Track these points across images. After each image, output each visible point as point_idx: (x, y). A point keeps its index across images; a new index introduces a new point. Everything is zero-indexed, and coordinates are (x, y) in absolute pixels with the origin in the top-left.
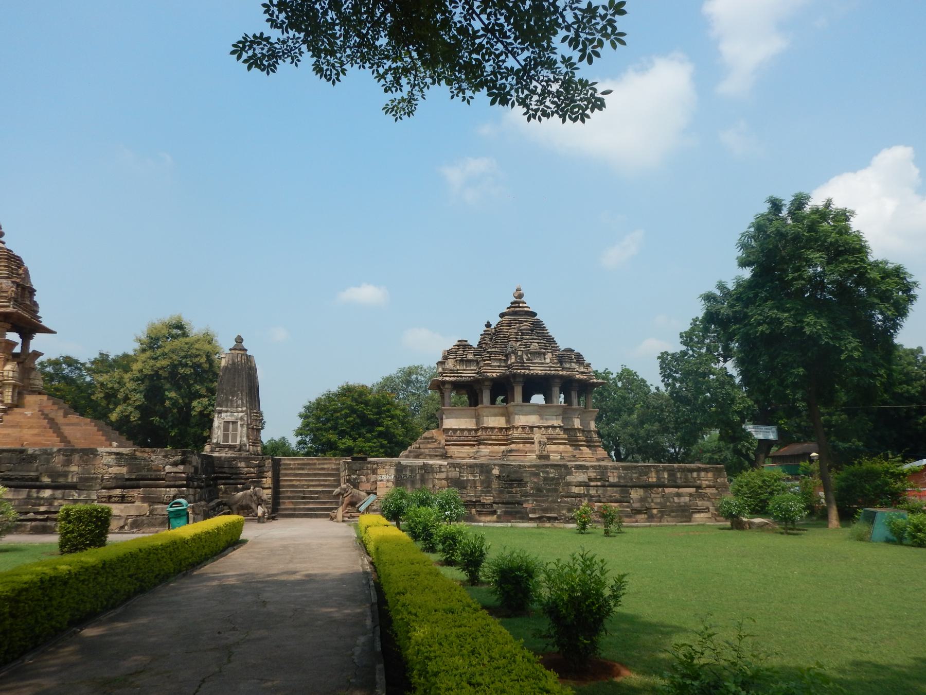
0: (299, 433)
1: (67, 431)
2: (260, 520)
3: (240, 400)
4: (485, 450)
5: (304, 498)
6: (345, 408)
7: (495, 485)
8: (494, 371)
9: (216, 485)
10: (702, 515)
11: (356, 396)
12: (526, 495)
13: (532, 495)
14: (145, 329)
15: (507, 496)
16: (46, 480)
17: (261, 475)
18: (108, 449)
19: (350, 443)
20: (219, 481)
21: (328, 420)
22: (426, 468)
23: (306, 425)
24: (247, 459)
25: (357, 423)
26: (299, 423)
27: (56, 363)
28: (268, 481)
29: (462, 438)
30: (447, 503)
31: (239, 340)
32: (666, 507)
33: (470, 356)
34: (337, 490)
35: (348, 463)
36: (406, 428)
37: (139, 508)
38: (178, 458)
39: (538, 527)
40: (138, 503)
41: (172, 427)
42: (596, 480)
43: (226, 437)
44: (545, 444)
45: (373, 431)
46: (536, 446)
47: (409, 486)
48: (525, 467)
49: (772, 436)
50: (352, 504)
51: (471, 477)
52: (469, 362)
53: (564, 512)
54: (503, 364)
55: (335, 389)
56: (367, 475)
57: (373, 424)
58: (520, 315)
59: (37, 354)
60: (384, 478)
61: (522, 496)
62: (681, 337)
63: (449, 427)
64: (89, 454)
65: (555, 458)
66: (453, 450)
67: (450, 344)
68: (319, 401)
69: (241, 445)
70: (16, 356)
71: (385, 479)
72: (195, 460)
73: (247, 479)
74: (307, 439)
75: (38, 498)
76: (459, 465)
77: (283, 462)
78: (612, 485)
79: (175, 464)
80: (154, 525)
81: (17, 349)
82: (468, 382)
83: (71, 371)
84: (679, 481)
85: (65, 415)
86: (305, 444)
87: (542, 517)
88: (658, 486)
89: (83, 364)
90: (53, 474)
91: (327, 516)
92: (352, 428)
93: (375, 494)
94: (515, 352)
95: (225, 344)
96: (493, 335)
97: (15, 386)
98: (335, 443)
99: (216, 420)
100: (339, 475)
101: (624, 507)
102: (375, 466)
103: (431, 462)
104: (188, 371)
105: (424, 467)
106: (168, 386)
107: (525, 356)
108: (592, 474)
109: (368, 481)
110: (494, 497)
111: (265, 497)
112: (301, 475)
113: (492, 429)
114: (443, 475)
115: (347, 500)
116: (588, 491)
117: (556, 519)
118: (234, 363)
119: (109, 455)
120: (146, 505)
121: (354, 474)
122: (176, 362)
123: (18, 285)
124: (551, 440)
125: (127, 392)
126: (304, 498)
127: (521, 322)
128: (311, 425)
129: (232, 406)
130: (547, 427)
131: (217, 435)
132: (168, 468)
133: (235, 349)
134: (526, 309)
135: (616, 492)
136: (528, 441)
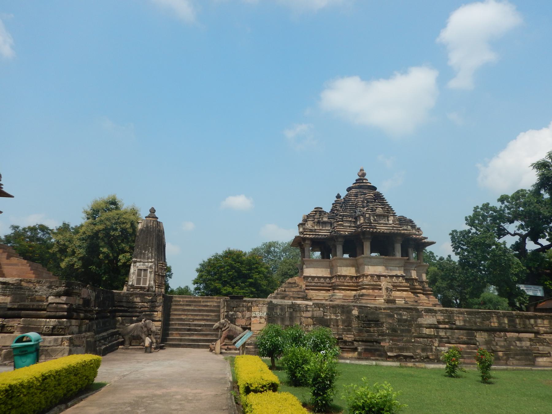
0: (195, 282)
2: (148, 350)
3: (150, 253)
4: (339, 294)
5: (189, 330)
6: (227, 266)
7: (355, 324)
8: (346, 229)
9: (114, 317)
10: (545, 359)
11: (235, 257)
12: (383, 334)
13: (388, 335)
15: (366, 334)
17: (153, 309)
19: (230, 289)
20: (117, 314)
21: (215, 274)
23: (200, 277)
24: (142, 296)
25: (235, 276)
26: (196, 275)
28: (158, 315)
29: (319, 284)
30: (322, 343)
31: (153, 211)
32: (510, 350)
33: (325, 219)
34: (217, 324)
35: (227, 301)
36: (268, 280)
38: (62, 289)
39: (401, 367)
41: (104, 273)
42: (444, 323)
43: (138, 281)
44: (391, 290)
45: (246, 282)
46: (384, 292)
47: (279, 323)
48: (380, 309)
49: (540, 294)
50: (230, 337)
51: (333, 317)
52: (325, 223)
53: (418, 351)
54: (353, 225)
55: (220, 252)
56: (243, 311)
57: (246, 277)
58: (363, 189)
60: (258, 315)
61: (379, 335)
62: (466, 220)
63: (308, 275)
65: (400, 302)
66: (312, 294)
67: (309, 210)
68: (210, 260)
69: (149, 287)
71: (258, 316)
73: (141, 312)
74: (201, 287)
76: (323, 306)
77: (175, 299)
79: (58, 295)
82: (324, 239)
83: (44, 235)
84: (518, 327)
85: (8, 257)
87: (399, 356)
88: (501, 331)
89: (51, 230)
91: (207, 347)
92: (232, 279)
93: (250, 329)
94: (363, 215)
95: (144, 213)
96: (341, 204)
98: (220, 289)
99: (132, 267)
101: (472, 349)
102: (250, 304)
103: (299, 302)
104: (117, 234)
105: (293, 307)
106: (102, 244)
107: (372, 218)
108: (441, 318)
109: (243, 317)
110: (354, 335)
111: (154, 329)
112: (188, 310)
113: (345, 276)
114: (309, 314)
115: (224, 334)
116: (438, 332)
117: (412, 357)
118: (147, 227)
121: (231, 311)
122: (109, 227)
124: (396, 287)
125: (74, 247)
126: (189, 330)
127: (365, 194)
128: (204, 277)
129: (144, 258)
130: (391, 277)
131: (132, 279)
132: (51, 299)
133: (149, 217)
134: (368, 184)
135: (463, 335)
136: (377, 287)
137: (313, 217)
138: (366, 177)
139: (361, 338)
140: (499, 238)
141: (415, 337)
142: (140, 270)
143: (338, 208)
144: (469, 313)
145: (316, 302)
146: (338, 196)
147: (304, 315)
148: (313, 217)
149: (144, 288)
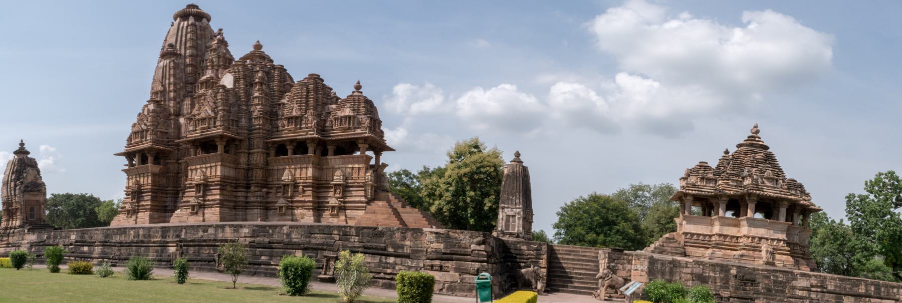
1: (404, 217)
7: (732, 282)
12: (758, 293)
14: (454, 147)
16: (391, 250)
17: (538, 257)
18: (430, 230)
23: (561, 221)
26: (556, 219)
27: (398, 174)
28: (543, 262)
31: (518, 155)
33: (710, 176)
37: (453, 276)
38: (480, 239)
40: (452, 273)
42: (817, 286)
43: (507, 226)
51: (712, 274)
52: (709, 180)
59: (385, 166)
62: (866, 184)
64: (418, 232)
65: (779, 265)
67: (693, 164)
70: (372, 166)
72: (491, 241)
75: (386, 263)
76: (701, 263)
78: (828, 292)
79: (479, 244)
80: (463, 291)
81: (373, 162)
84: (882, 294)
85: (403, 207)
90: (396, 246)
95: (507, 159)
97: (372, 186)
99: (500, 213)
100: (597, 262)
103: (679, 258)
105: (674, 263)
107: (760, 180)
108: (814, 282)
114: (689, 270)
118: (513, 172)
119: (431, 238)
120: (457, 274)
123: (371, 119)
129: (512, 204)
130: (773, 240)
131: (501, 224)
132: (473, 247)
133: (514, 161)
137: (697, 171)
138: (759, 135)
139: (736, 295)
140: (896, 207)
141: (788, 297)
142: (508, 216)
143: (725, 164)
144: (840, 280)
145: (695, 259)
146: (727, 152)
147: (685, 270)
148: (697, 171)
149: (514, 234)
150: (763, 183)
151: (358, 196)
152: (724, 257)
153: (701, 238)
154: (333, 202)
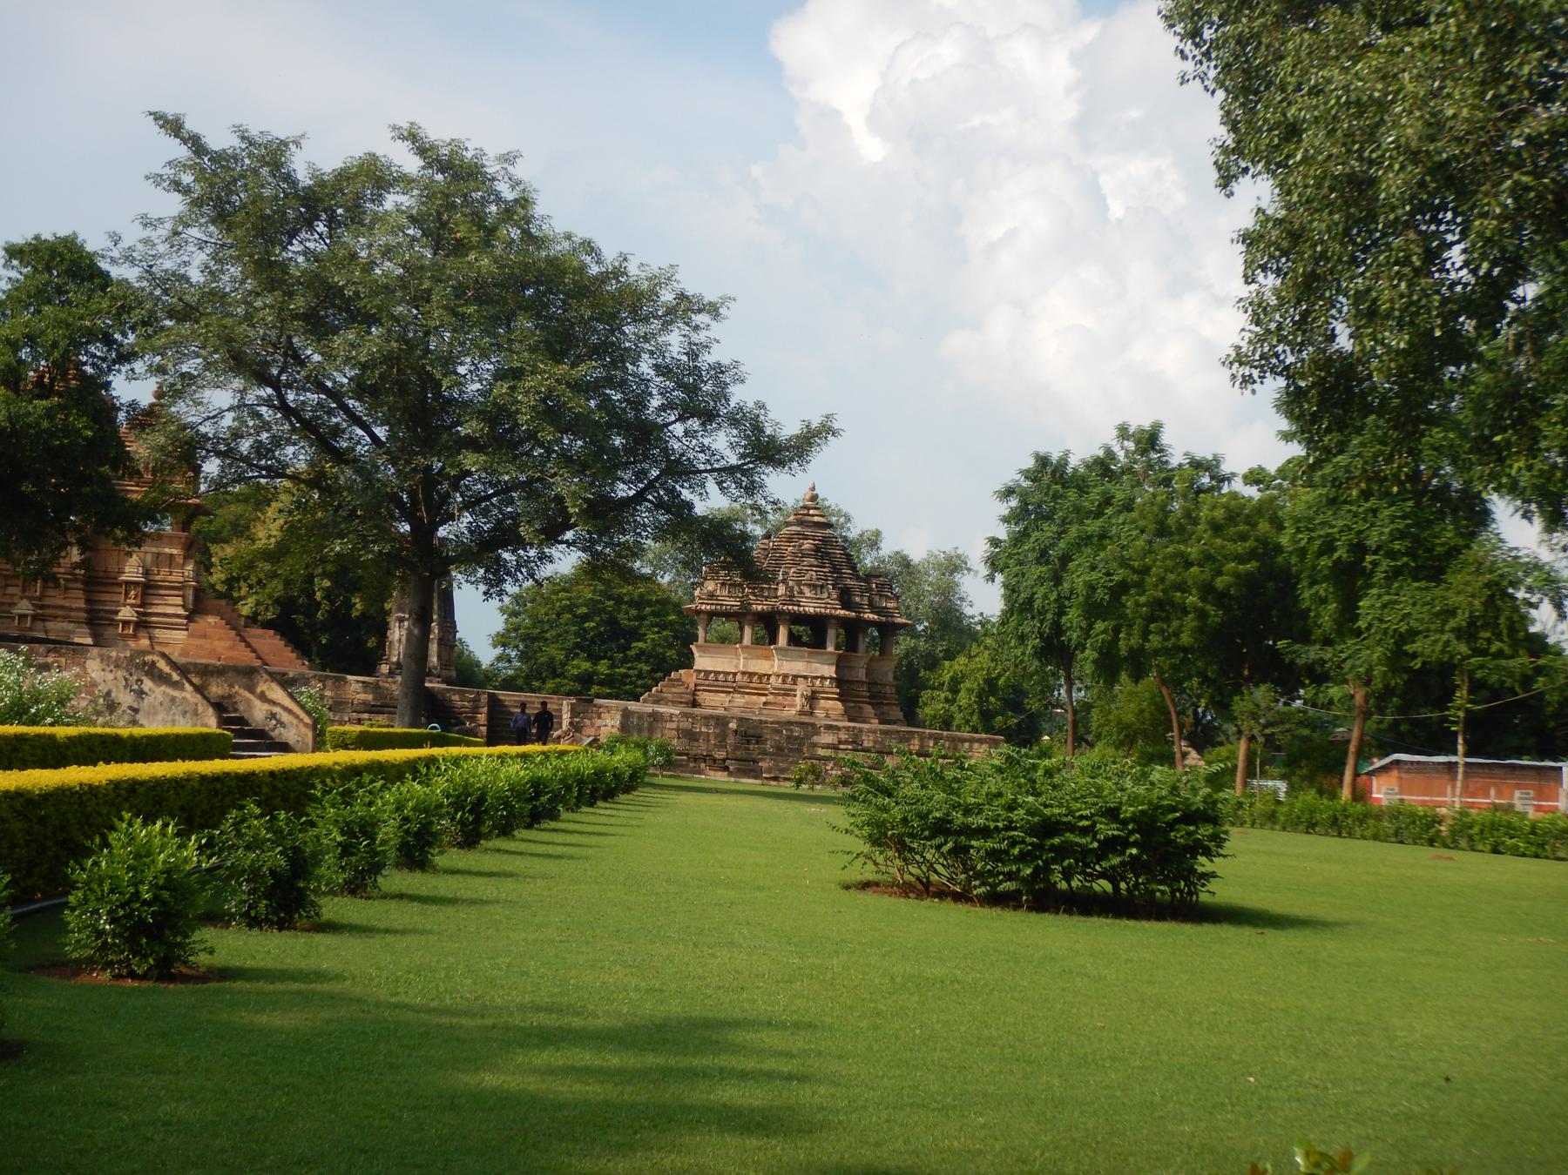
1: (255, 642)
7: (731, 740)
12: (765, 753)
17: (475, 710)
22: (655, 716)
25: (601, 634)
42: (846, 742)
86: (509, 661)
105: (654, 715)
108: (844, 736)
114: (674, 725)
147: (669, 725)
150: (801, 592)
151: (171, 606)
152: (746, 707)
153: (721, 677)
154: (126, 613)
